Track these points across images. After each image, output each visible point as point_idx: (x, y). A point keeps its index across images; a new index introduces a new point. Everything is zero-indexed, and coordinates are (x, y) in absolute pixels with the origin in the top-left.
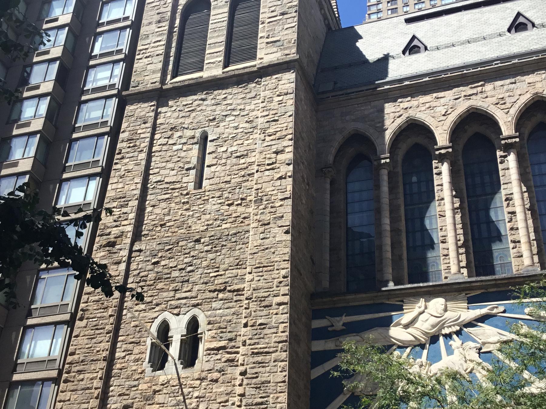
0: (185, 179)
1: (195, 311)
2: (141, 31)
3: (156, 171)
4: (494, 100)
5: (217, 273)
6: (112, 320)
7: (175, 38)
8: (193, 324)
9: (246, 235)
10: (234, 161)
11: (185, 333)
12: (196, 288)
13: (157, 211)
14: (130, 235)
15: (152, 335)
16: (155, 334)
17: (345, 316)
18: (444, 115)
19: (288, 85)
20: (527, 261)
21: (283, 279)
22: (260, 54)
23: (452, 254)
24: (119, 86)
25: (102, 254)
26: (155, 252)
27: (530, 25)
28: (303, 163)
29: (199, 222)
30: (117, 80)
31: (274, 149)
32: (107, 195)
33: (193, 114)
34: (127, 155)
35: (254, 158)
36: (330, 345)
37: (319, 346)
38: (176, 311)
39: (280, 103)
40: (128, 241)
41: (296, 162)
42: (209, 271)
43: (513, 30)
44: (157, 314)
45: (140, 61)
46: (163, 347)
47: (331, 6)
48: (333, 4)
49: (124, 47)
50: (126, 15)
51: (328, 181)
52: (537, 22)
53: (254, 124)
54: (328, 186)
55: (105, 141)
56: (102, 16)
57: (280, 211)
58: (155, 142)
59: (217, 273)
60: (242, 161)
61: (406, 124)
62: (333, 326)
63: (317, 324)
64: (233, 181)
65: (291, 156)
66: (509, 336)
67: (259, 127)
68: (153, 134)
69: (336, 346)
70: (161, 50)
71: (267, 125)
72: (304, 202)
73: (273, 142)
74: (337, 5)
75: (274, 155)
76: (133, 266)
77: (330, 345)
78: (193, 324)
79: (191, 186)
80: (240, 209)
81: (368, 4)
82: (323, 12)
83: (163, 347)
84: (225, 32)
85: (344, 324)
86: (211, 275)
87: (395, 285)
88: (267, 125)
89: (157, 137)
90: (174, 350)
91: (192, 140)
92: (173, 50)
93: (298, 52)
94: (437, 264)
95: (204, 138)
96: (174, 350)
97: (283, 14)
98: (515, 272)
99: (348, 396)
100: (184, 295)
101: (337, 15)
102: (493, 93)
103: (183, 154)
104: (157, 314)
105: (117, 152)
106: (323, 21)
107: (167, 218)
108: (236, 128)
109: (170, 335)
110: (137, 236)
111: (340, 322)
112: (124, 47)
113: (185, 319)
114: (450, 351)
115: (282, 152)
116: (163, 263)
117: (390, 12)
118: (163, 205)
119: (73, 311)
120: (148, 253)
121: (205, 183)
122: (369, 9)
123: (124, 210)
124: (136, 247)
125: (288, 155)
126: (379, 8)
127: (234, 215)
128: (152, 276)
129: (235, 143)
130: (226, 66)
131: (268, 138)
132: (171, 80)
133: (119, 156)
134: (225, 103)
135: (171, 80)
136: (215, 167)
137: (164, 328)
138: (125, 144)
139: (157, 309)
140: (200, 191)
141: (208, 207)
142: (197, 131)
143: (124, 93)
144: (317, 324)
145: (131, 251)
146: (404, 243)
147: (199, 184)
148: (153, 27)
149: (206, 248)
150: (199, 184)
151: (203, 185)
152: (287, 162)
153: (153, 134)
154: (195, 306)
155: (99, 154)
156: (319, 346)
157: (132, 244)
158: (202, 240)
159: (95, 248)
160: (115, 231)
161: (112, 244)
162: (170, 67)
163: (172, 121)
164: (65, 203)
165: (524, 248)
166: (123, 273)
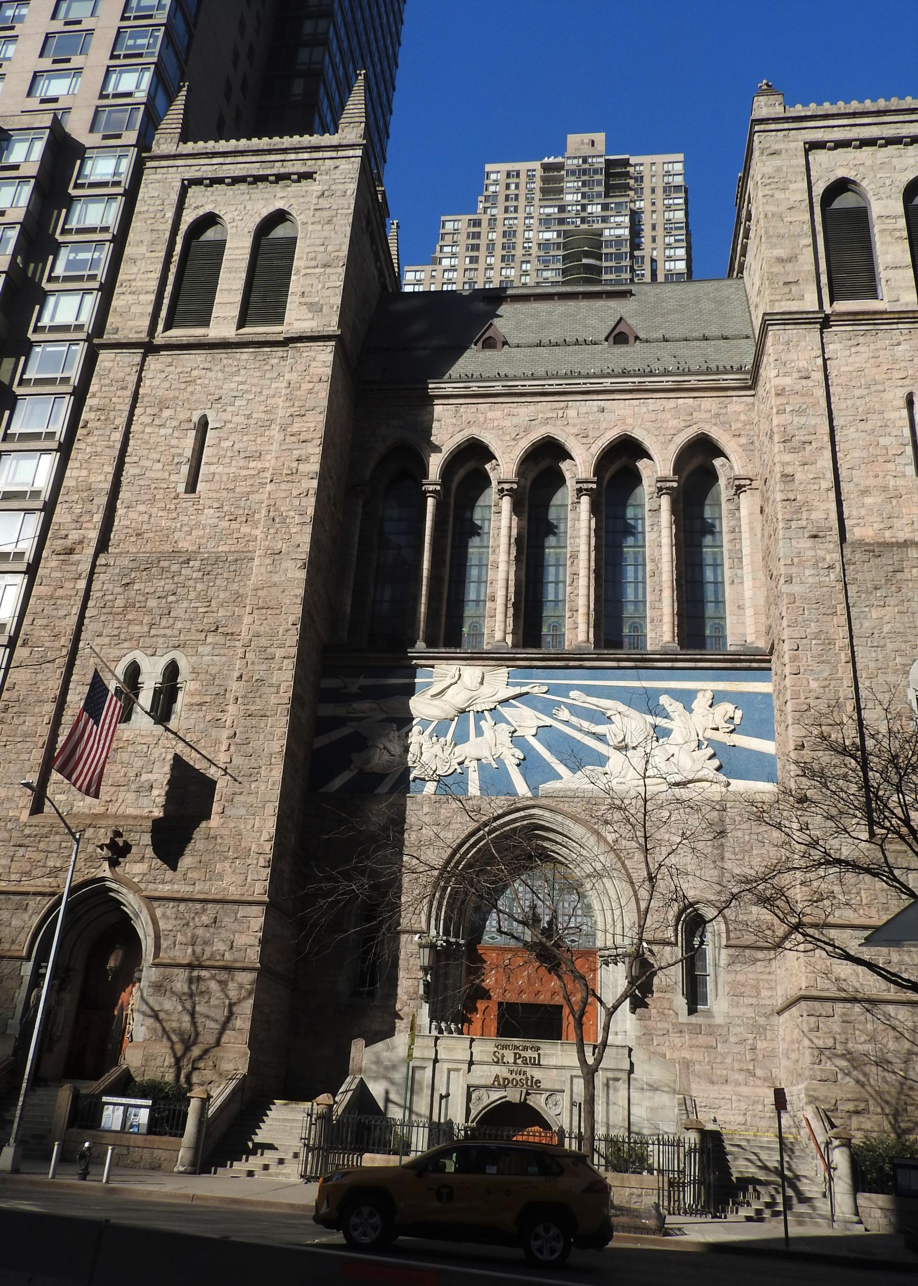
0: (174, 478)
1: (177, 655)
2: (126, 253)
3: (136, 459)
4: (575, 431)
5: (208, 609)
6: (64, 652)
7: (173, 269)
8: (172, 671)
9: (250, 565)
10: (242, 463)
11: (160, 680)
12: (179, 625)
13: (133, 515)
14: (94, 543)
15: (117, 679)
16: (122, 678)
17: (364, 677)
18: (514, 439)
19: (322, 370)
20: (582, 637)
21: (291, 627)
22: (289, 315)
23: (500, 617)
24: (88, 328)
25: (54, 564)
26: (126, 571)
27: (631, 339)
28: (331, 478)
29: (188, 538)
30: (87, 317)
31: (296, 453)
32: (64, 484)
33: (190, 389)
34: (96, 432)
35: (269, 462)
36: (341, 711)
37: (327, 710)
38: (150, 651)
39: (310, 391)
40: (91, 551)
41: (323, 476)
42: (197, 605)
43: (611, 339)
44: (125, 651)
45: (122, 297)
46: (131, 695)
47: (390, 255)
48: (392, 253)
49: (123, 178)
50: (104, 225)
51: (361, 502)
52: (642, 335)
53: (273, 417)
54: (360, 510)
55: (67, 403)
56: (69, 220)
57: (298, 539)
58: (96, 575)
59: (208, 609)
60: (252, 464)
61: (467, 443)
62: (346, 688)
63: (329, 683)
64: (238, 489)
65: (316, 468)
66: (548, 721)
67: (278, 421)
68: (133, 407)
69: (349, 713)
70: (154, 285)
71: (289, 420)
72: (327, 528)
73: (296, 446)
74: (398, 255)
75: (295, 464)
76: (96, 586)
77: (341, 711)
78: (172, 671)
79: (181, 488)
80: (245, 529)
81: (442, 231)
82: (379, 265)
83: (131, 695)
84: (244, 275)
85: (360, 688)
86: (200, 610)
87: (428, 646)
88: (289, 420)
89: (137, 411)
90: (145, 698)
91: (186, 424)
92: (169, 289)
93: (340, 326)
94: (481, 626)
95: (203, 426)
96: (145, 698)
97: (326, 266)
98: (566, 648)
99: (355, 773)
100: (162, 632)
101: (396, 270)
102: (575, 421)
103: (174, 442)
104: (125, 651)
105: (81, 424)
106: (377, 278)
107: (145, 527)
108: (249, 417)
109: (139, 681)
110: (103, 545)
111: (356, 684)
112: (123, 178)
113: (161, 663)
114: (479, 732)
115: (307, 460)
116: (136, 587)
117: (468, 260)
118: (142, 508)
119: (12, 634)
120: (117, 571)
121: (200, 486)
122: (442, 239)
123: (88, 506)
124: (101, 560)
125: (314, 466)
126: (455, 239)
127: (235, 535)
128: (120, 602)
129: (245, 438)
130: (241, 325)
131: (289, 439)
132: (163, 332)
133: (84, 431)
134: (236, 379)
135: (163, 332)
136: (215, 466)
137: (134, 671)
138: (92, 415)
139: (126, 645)
140: (193, 496)
141: (202, 518)
142: (194, 413)
143: (96, 341)
144: (329, 683)
145: (94, 566)
146: (445, 596)
147: (191, 487)
148: (143, 249)
149: (195, 575)
150: (191, 487)
151: (198, 489)
152: (310, 476)
153: (133, 407)
154: (176, 647)
155: (55, 422)
156: (327, 710)
157: (96, 556)
158: (191, 563)
159: (44, 554)
160: (74, 536)
161: (70, 551)
162: (163, 313)
163: (160, 392)
164: (78, 223)
165: (581, 619)
166: (82, 593)
